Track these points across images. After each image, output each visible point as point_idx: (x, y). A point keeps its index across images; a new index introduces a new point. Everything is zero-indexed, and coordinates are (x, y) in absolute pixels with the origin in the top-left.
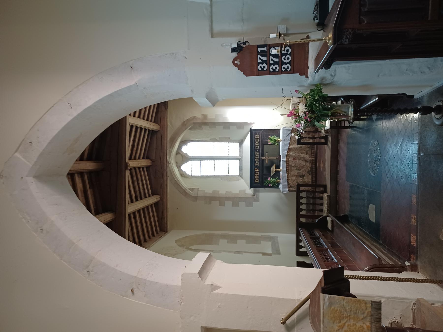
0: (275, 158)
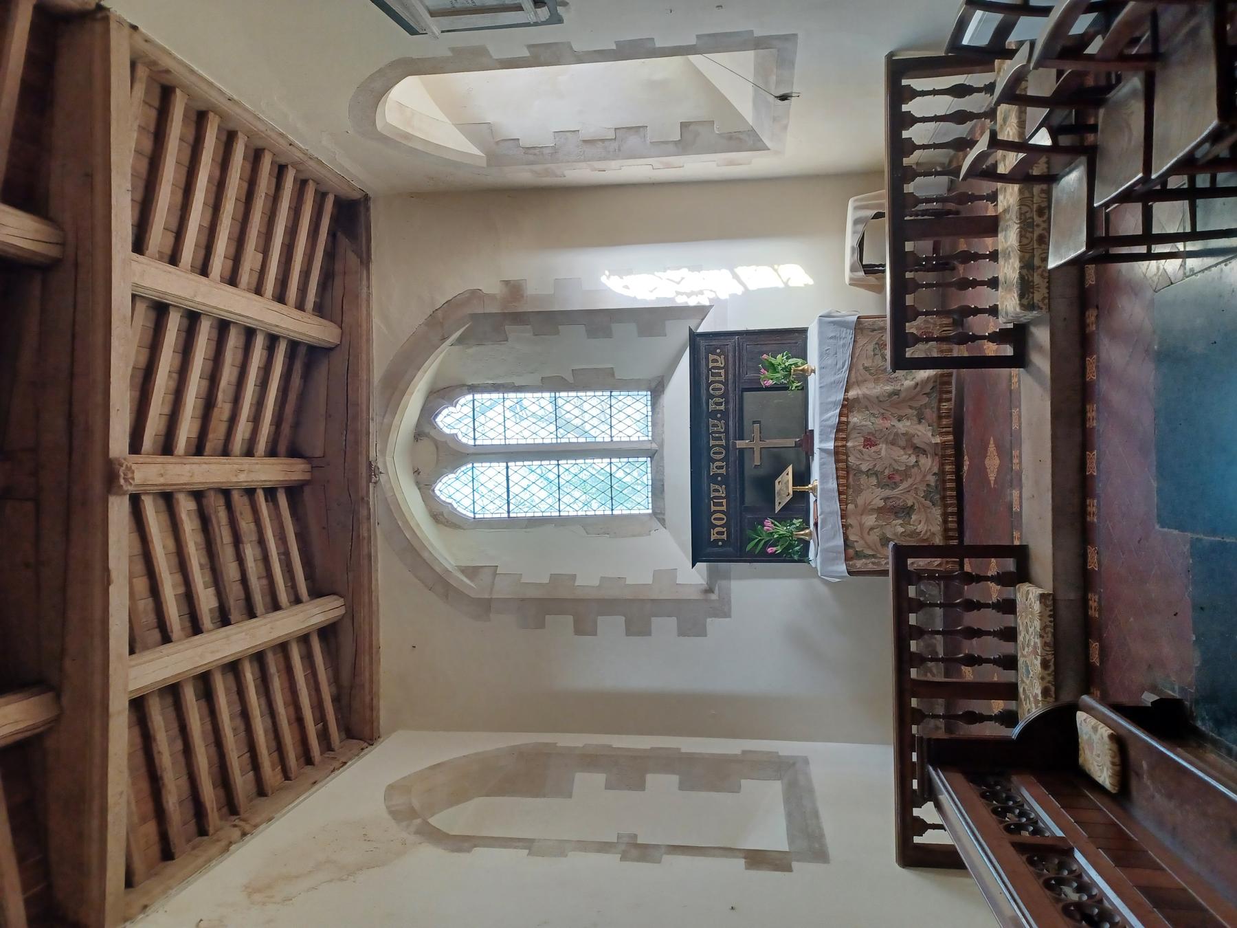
0: (790, 442)
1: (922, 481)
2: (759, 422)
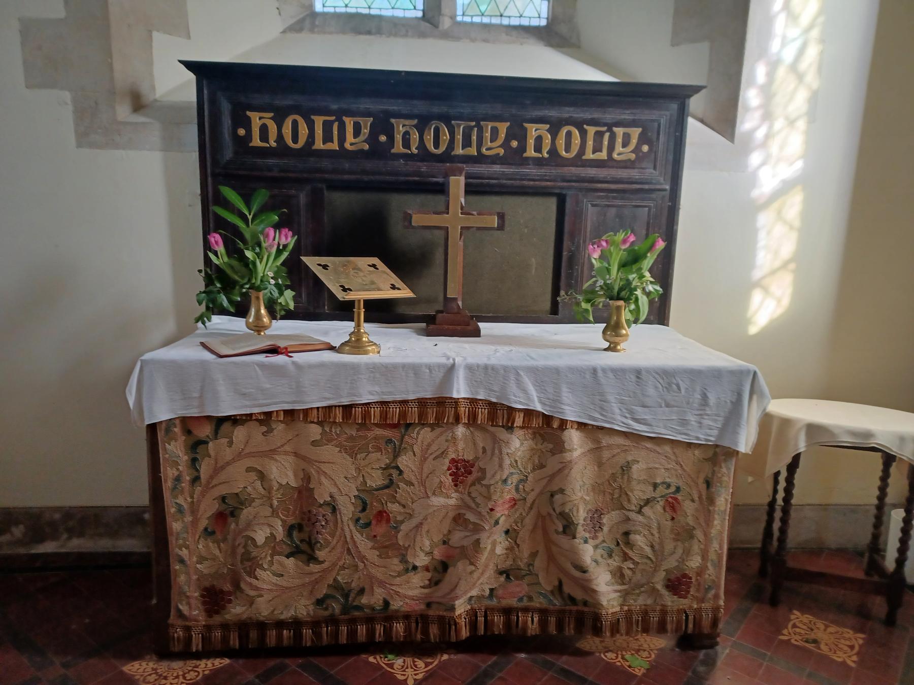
1: (371, 577)
2: (501, 227)
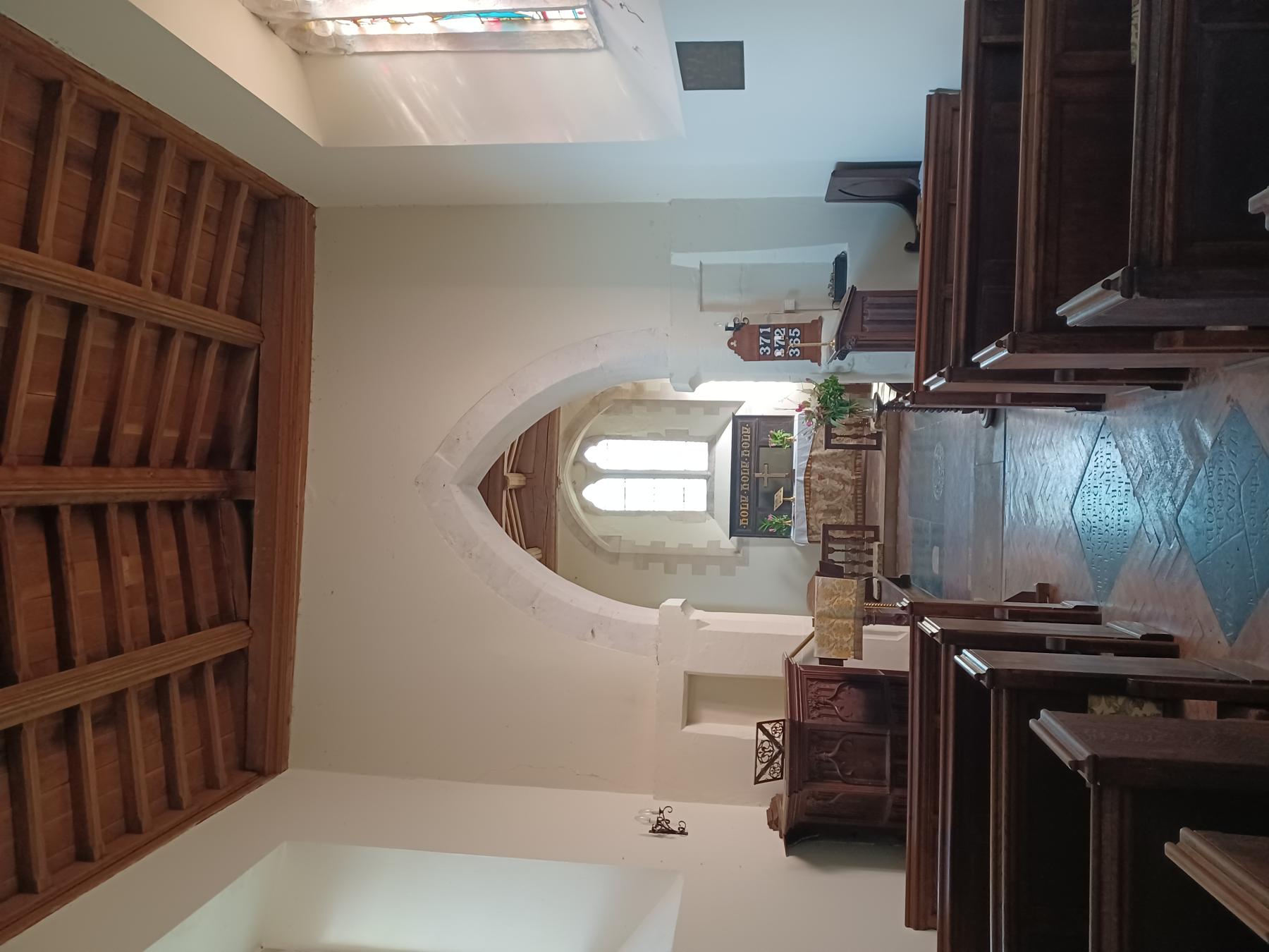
0: (783, 475)
